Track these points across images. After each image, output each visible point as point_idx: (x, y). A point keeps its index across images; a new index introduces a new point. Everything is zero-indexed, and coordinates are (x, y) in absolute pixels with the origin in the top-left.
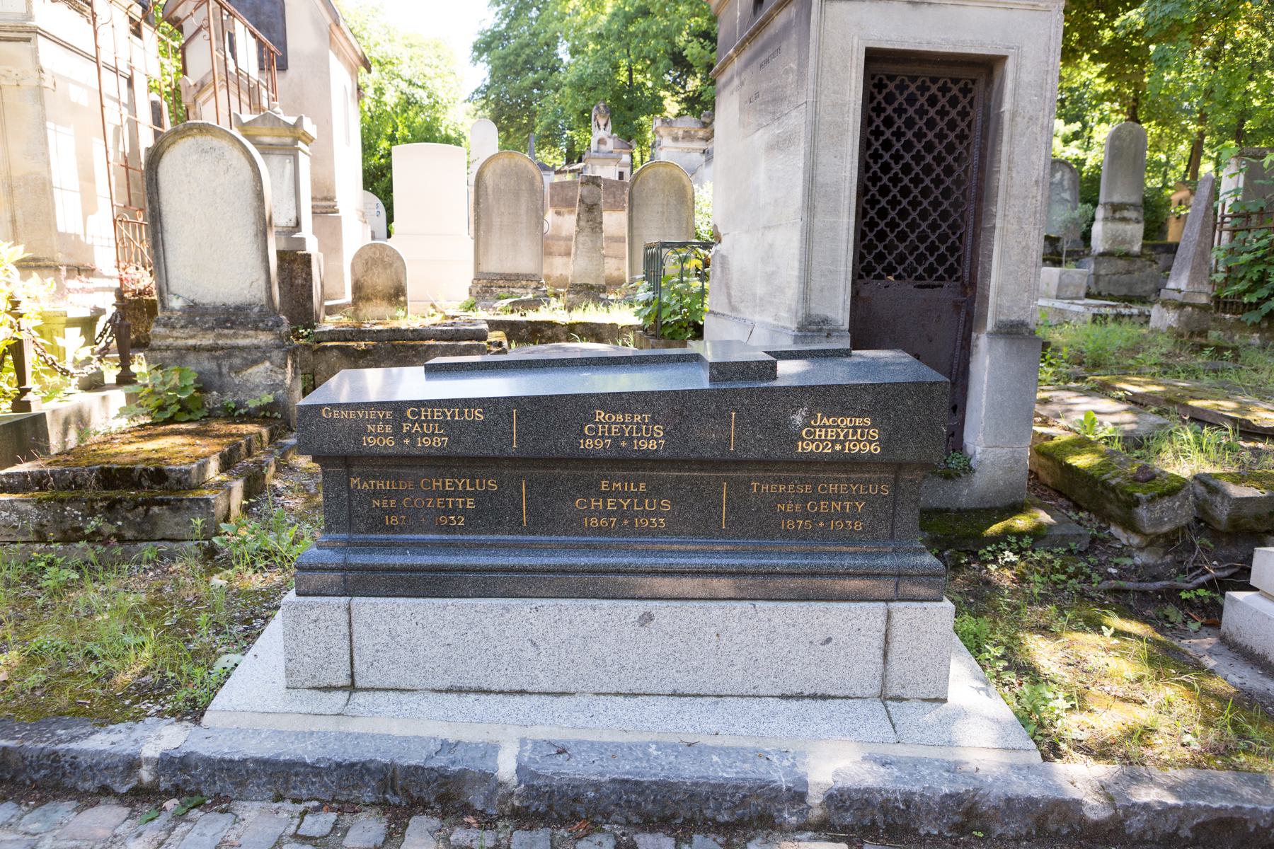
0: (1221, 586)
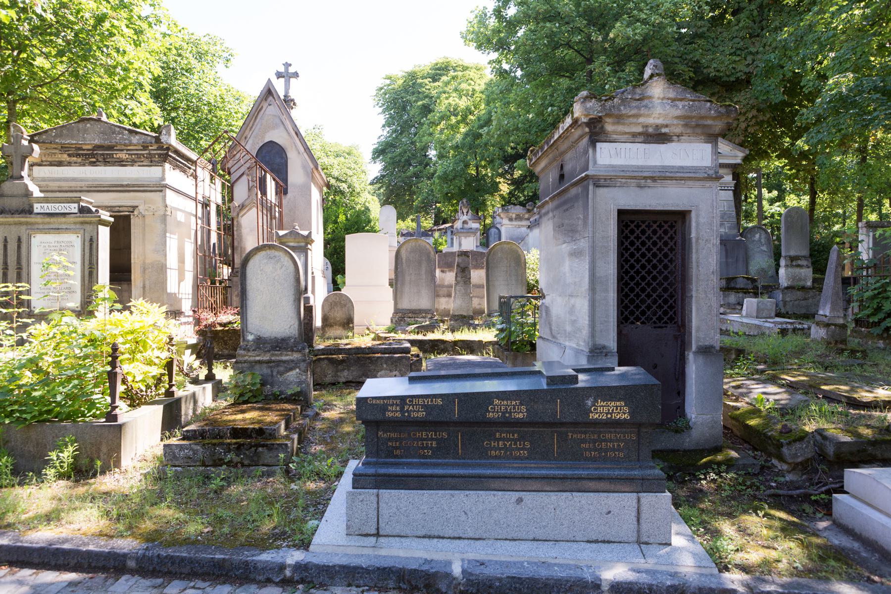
0: (829, 492)
